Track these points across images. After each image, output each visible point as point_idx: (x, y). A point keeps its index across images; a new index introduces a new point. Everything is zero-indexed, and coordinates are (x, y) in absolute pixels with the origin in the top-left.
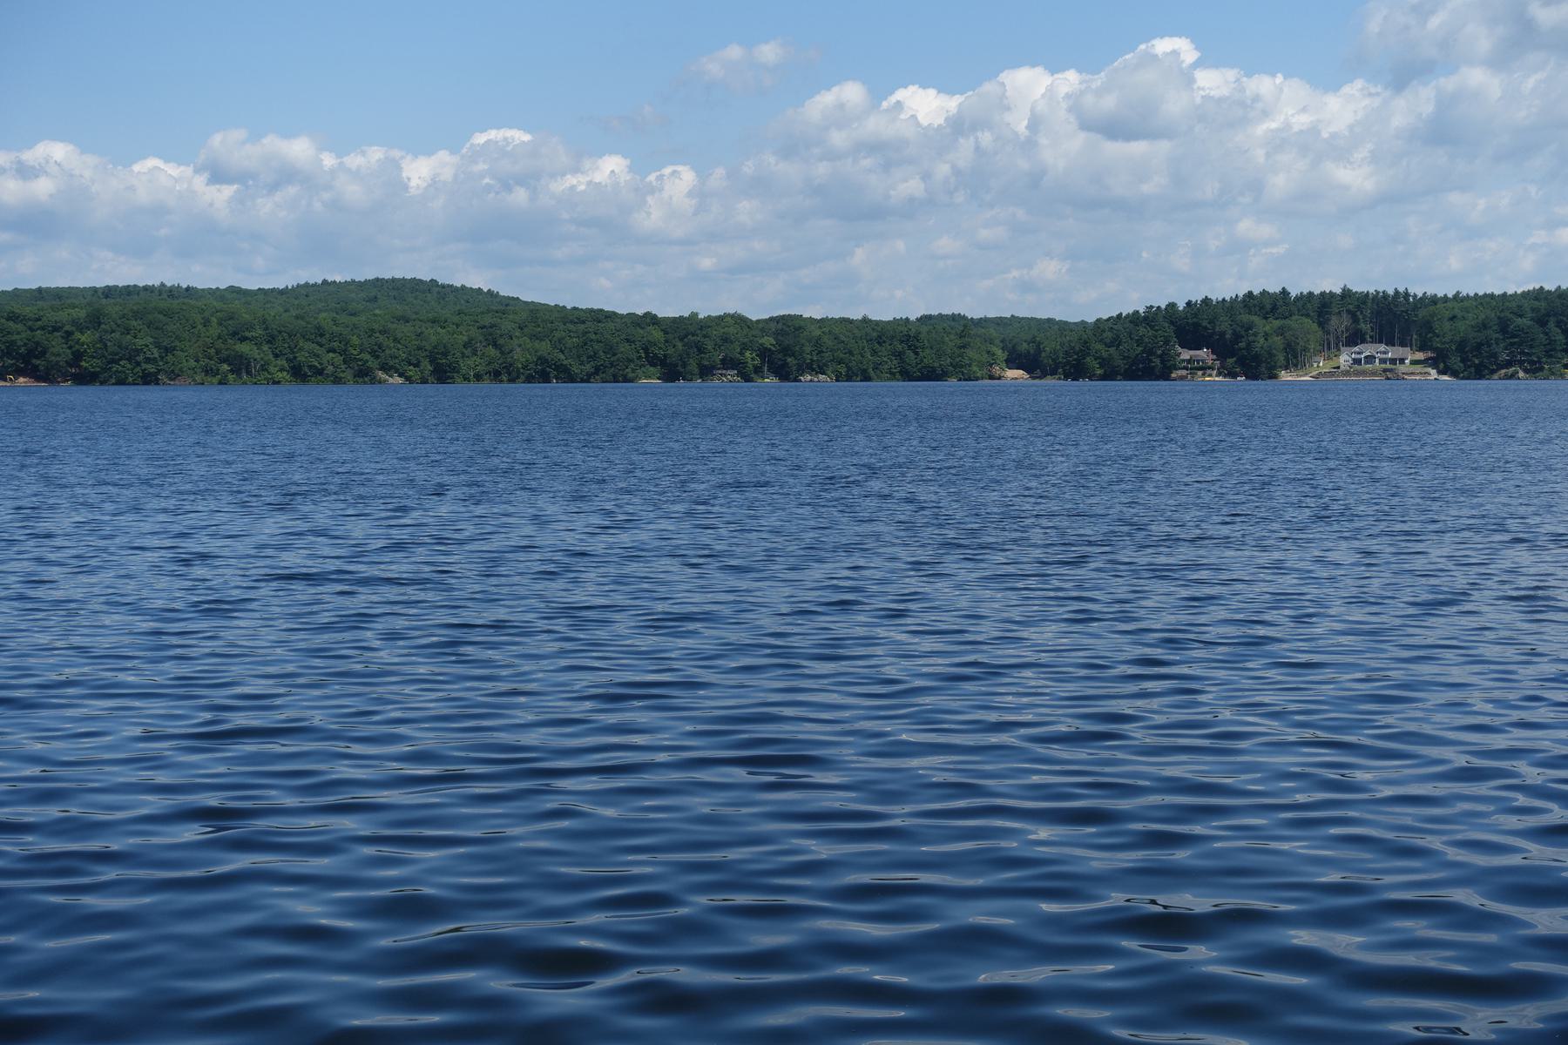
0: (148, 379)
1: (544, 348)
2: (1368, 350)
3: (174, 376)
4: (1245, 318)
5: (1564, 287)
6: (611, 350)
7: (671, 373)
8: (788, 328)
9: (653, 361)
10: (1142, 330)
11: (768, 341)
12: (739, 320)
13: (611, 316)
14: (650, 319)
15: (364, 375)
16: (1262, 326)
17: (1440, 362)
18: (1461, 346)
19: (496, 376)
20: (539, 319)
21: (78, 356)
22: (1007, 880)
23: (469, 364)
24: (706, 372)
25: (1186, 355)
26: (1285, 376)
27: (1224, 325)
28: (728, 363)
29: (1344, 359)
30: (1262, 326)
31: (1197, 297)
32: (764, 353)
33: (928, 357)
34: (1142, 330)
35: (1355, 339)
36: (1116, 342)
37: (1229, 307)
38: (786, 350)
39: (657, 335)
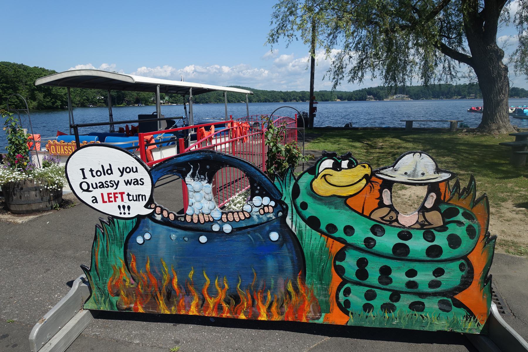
0: (207, 103)
1: (266, 97)
2: (399, 95)
3: (210, 102)
4: (378, 90)
5: (526, 89)
6: (276, 97)
7: (285, 101)
8: (287, 93)
9: (282, 99)
10: (361, 93)
11: (301, 95)
12: (295, 92)
13: (275, 91)
14: (281, 92)
15: (239, 101)
16: (381, 92)
17: (411, 97)
18: (415, 95)
19: (258, 101)
20: (264, 92)
21: (196, 99)
22: (35, 331)
23: (254, 100)
24: (291, 100)
25: (368, 97)
26: (385, 100)
27: (375, 92)
28: (294, 99)
29: (395, 97)
30: (381, 92)
31: (369, 87)
32: (300, 97)
33: (326, 98)
34: (361, 93)
35: (395, 94)
36: (357, 95)
37: (376, 88)
38: (303, 97)
39: (283, 94)
